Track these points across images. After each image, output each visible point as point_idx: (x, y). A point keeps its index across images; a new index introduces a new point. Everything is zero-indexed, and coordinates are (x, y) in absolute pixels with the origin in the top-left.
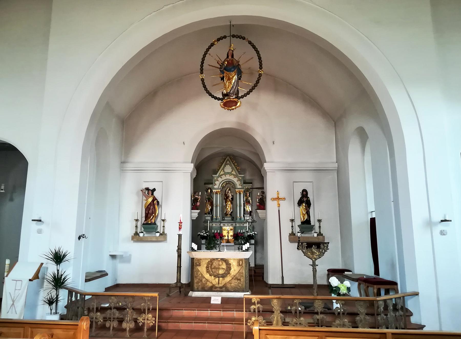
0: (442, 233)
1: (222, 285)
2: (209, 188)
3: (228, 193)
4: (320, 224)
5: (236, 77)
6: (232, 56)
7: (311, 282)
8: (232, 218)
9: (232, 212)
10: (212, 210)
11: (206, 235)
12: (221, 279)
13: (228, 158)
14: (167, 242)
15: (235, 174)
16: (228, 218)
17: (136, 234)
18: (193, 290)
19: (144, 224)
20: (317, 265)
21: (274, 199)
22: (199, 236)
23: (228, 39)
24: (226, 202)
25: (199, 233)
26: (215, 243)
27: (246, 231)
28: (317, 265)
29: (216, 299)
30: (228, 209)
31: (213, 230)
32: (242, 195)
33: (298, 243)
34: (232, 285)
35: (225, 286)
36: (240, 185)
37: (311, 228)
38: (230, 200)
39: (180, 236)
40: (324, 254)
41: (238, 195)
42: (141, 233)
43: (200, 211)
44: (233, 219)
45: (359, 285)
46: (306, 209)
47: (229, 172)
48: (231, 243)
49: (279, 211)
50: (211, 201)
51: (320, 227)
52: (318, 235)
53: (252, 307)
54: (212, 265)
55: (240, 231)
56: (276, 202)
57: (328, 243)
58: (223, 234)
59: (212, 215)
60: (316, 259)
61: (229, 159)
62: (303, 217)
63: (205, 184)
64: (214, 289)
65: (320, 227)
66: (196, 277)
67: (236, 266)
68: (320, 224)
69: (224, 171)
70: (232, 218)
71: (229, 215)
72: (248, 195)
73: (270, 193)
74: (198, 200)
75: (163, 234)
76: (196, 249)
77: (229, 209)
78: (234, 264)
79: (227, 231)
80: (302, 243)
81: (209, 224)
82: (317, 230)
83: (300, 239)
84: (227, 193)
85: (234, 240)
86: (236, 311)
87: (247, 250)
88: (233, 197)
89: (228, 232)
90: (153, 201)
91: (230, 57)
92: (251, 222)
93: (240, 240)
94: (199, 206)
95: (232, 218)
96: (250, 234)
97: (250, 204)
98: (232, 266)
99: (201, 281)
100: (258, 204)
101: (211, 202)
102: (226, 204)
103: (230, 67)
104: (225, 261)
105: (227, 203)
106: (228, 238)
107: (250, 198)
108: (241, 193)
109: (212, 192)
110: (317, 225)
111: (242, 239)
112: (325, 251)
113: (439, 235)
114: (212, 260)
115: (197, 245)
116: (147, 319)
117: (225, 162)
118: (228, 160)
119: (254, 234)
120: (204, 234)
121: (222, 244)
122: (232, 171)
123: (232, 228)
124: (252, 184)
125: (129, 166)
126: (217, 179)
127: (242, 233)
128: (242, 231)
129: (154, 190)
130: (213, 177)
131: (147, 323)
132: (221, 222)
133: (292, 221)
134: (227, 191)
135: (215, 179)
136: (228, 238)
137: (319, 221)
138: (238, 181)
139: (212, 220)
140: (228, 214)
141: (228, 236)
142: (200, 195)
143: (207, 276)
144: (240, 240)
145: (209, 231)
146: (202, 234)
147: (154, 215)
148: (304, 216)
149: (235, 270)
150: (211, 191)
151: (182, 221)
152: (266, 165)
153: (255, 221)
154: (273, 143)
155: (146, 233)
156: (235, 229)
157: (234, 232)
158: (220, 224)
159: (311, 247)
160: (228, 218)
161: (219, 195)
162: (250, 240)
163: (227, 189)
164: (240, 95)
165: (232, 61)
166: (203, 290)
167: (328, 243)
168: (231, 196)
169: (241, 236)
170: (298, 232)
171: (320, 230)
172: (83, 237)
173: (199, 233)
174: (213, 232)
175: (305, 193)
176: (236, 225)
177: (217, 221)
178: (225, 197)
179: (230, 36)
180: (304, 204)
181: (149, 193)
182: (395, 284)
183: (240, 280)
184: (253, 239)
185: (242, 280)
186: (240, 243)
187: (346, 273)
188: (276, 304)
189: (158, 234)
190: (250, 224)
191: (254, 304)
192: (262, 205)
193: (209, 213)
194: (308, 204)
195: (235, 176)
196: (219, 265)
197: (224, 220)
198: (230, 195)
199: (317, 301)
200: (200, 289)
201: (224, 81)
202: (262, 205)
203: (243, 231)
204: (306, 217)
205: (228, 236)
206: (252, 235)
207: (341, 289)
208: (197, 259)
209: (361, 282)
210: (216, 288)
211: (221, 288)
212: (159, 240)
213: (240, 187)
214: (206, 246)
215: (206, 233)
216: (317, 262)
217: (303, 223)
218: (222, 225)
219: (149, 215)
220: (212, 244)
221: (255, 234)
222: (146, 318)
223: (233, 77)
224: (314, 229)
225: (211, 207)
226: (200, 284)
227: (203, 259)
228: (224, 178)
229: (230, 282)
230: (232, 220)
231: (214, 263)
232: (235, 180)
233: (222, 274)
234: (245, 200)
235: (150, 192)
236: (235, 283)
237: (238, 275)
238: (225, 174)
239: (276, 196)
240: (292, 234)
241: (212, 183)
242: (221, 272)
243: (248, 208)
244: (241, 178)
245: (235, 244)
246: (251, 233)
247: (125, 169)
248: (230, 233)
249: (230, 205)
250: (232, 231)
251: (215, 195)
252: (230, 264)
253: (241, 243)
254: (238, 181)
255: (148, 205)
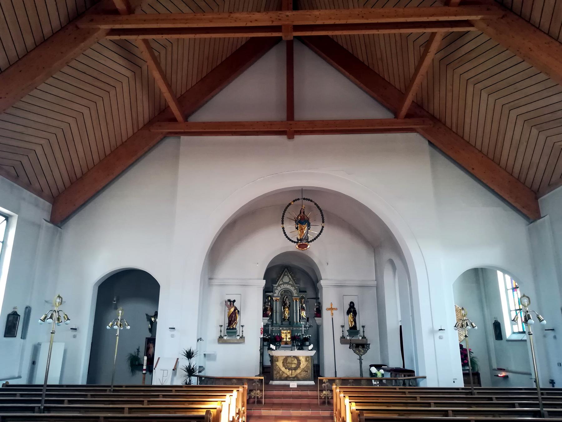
0: (441, 338)
1: (294, 376)
3: (286, 300)
4: (364, 329)
5: (306, 228)
6: (304, 213)
7: (358, 375)
12: (293, 371)
13: (286, 269)
14: (244, 344)
15: (292, 283)
17: (221, 337)
18: (273, 380)
20: (363, 359)
23: (301, 200)
28: (363, 359)
29: (293, 384)
33: (350, 344)
34: (302, 375)
35: (296, 376)
36: (296, 293)
37: (357, 333)
38: (288, 307)
40: (367, 351)
45: (391, 374)
46: (353, 317)
47: (287, 282)
49: (332, 318)
51: (364, 332)
52: (362, 338)
53: (323, 385)
54: (286, 361)
55: (297, 334)
56: (330, 312)
57: (370, 344)
60: (362, 355)
61: (287, 271)
62: (351, 324)
64: (288, 379)
65: (364, 332)
66: (275, 370)
67: (304, 361)
68: (364, 329)
69: (282, 281)
72: (303, 302)
73: (325, 305)
75: (242, 337)
76: (275, 349)
77: (286, 315)
78: (303, 360)
79: (285, 334)
80: (352, 344)
82: (361, 334)
83: (352, 341)
86: (309, 391)
87: (311, 350)
90: (235, 310)
91: (302, 214)
96: (306, 337)
97: (305, 310)
98: (301, 361)
99: (279, 373)
100: (315, 312)
103: (303, 221)
104: (297, 358)
108: (298, 300)
110: (361, 330)
112: (368, 350)
113: (438, 338)
114: (286, 358)
115: (275, 346)
116: (257, 394)
117: (284, 273)
120: (266, 336)
122: (289, 282)
124: (306, 292)
125: (215, 282)
126: (276, 288)
129: (234, 301)
130: (273, 287)
131: (257, 396)
133: (343, 326)
134: (285, 299)
137: (363, 327)
138: (294, 290)
141: (286, 339)
143: (283, 369)
147: (235, 322)
149: (303, 364)
154: (328, 264)
156: (292, 333)
157: (291, 335)
159: (359, 347)
164: (309, 240)
165: (304, 216)
166: (281, 379)
167: (370, 344)
168: (288, 303)
169: (298, 338)
170: (348, 336)
171: (364, 334)
172: (201, 340)
175: (352, 305)
176: (293, 329)
179: (302, 199)
180: (352, 314)
182: (413, 372)
183: (307, 372)
184: (308, 341)
185: (309, 372)
187: (383, 367)
188: (338, 382)
189: (238, 338)
191: (324, 383)
192: (319, 313)
194: (355, 314)
195: (292, 286)
196: (292, 361)
198: (288, 302)
199: (363, 380)
200: (278, 379)
201: (298, 230)
203: (299, 334)
204: (353, 324)
205: (286, 339)
207: (378, 375)
208: (275, 356)
209: (392, 372)
210: (290, 378)
211: (294, 378)
215: (268, 336)
216: (362, 357)
217: (351, 328)
219: (232, 322)
221: (309, 337)
222: (256, 393)
223: (305, 228)
224: (360, 333)
226: (278, 375)
227: (280, 356)
228: (282, 287)
229: (300, 374)
230: (290, 324)
231: (288, 360)
232: (292, 289)
233: (294, 368)
235: (231, 302)
236: (304, 374)
237: (306, 368)
239: (330, 307)
240: (343, 337)
241: (272, 292)
242: (294, 366)
244: (297, 287)
246: (306, 336)
249: (288, 312)
252: (300, 360)
254: (294, 290)
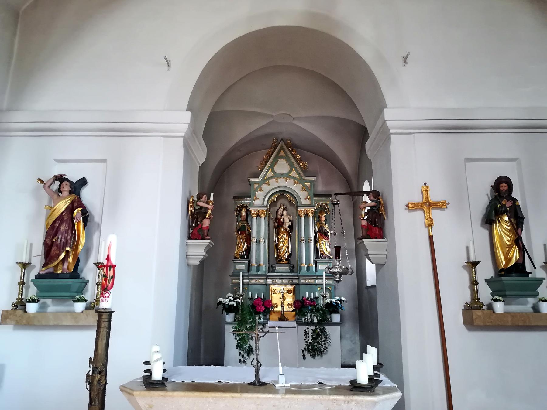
2: (243, 207)
8: (290, 267)
9: (289, 256)
10: (248, 250)
11: (235, 304)
16: (283, 268)
17: (20, 304)
19: (39, 276)
21: (412, 207)
22: (221, 306)
24: (278, 234)
25: (221, 299)
26: (254, 321)
27: (323, 296)
30: (282, 249)
31: (250, 293)
32: (311, 219)
38: (286, 230)
39: (104, 317)
41: (303, 218)
42: (29, 302)
43: (209, 241)
44: (292, 268)
47: (285, 172)
48: (287, 320)
49: (431, 238)
50: (247, 232)
55: (310, 295)
56: (419, 215)
58: (271, 301)
59: (250, 262)
63: (235, 197)
69: (273, 171)
70: (291, 268)
71: (284, 261)
72: (324, 219)
74: (206, 213)
77: (284, 248)
79: (281, 295)
81: (243, 280)
84: (279, 217)
85: (296, 315)
88: (292, 224)
89: (283, 297)
90: (70, 209)
92: (341, 274)
93: (309, 315)
94: (208, 229)
95: (291, 268)
96: (331, 302)
97: (328, 238)
101: (248, 234)
102: (278, 239)
105: (280, 237)
106: (283, 309)
107: (326, 227)
108: (310, 214)
109: (249, 215)
111: (314, 313)
118: (282, 148)
119: (339, 302)
120: (230, 301)
121: (270, 323)
123: (290, 288)
127: (312, 299)
128: (312, 294)
129: (83, 182)
130: (250, 184)
132: (268, 276)
134: (279, 212)
135: (255, 187)
136: (283, 309)
139: (249, 270)
140: (281, 260)
141: (283, 307)
142: (211, 202)
144: (309, 315)
145: (242, 296)
146: (226, 301)
147: (68, 249)
148: (509, 251)
150: (246, 213)
151: (113, 261)
152: (388, 114)
153: (350, 270)
154: (405, 62)
155: (52, 302)
156: (297, 289)
158: (266, 279)
160: (283, 268)
161: (263, 219)
162: (330, 314)
163: (280, 207)
168: (288, 221)
169: (311, 306)
173: (221, 299)
174: (250, 296)
177: (259, 273)
178: (277, 224)
180: (506, 218)
181: (61, 189)
184: (336, 312)
186: (310, 320)
190: (338, 277)
193: (242, 258)
197: (274, 271)
202: (375, 226)
205: (283, 307)
206: (334, 304)
212: (80, 324)
213: (308, 202)
214: (236, 328)
218: (269, 281)
219: (54, 250)
220: (247, 324)
225: (247, 244)
228: (273, 184)
230: (292, 271)
232: (297, 189)
234: (317, 230)
238: (276, 176)
239: (418, 198)
241: (249, 197)
243: (323, 246)
245: (299, 324)
246: (332, 300)
247: (6, 126)
248: (287, 300)
250: (291, 295)
251: (254, 219)
253: (312, 321)
255: (55, 222)
